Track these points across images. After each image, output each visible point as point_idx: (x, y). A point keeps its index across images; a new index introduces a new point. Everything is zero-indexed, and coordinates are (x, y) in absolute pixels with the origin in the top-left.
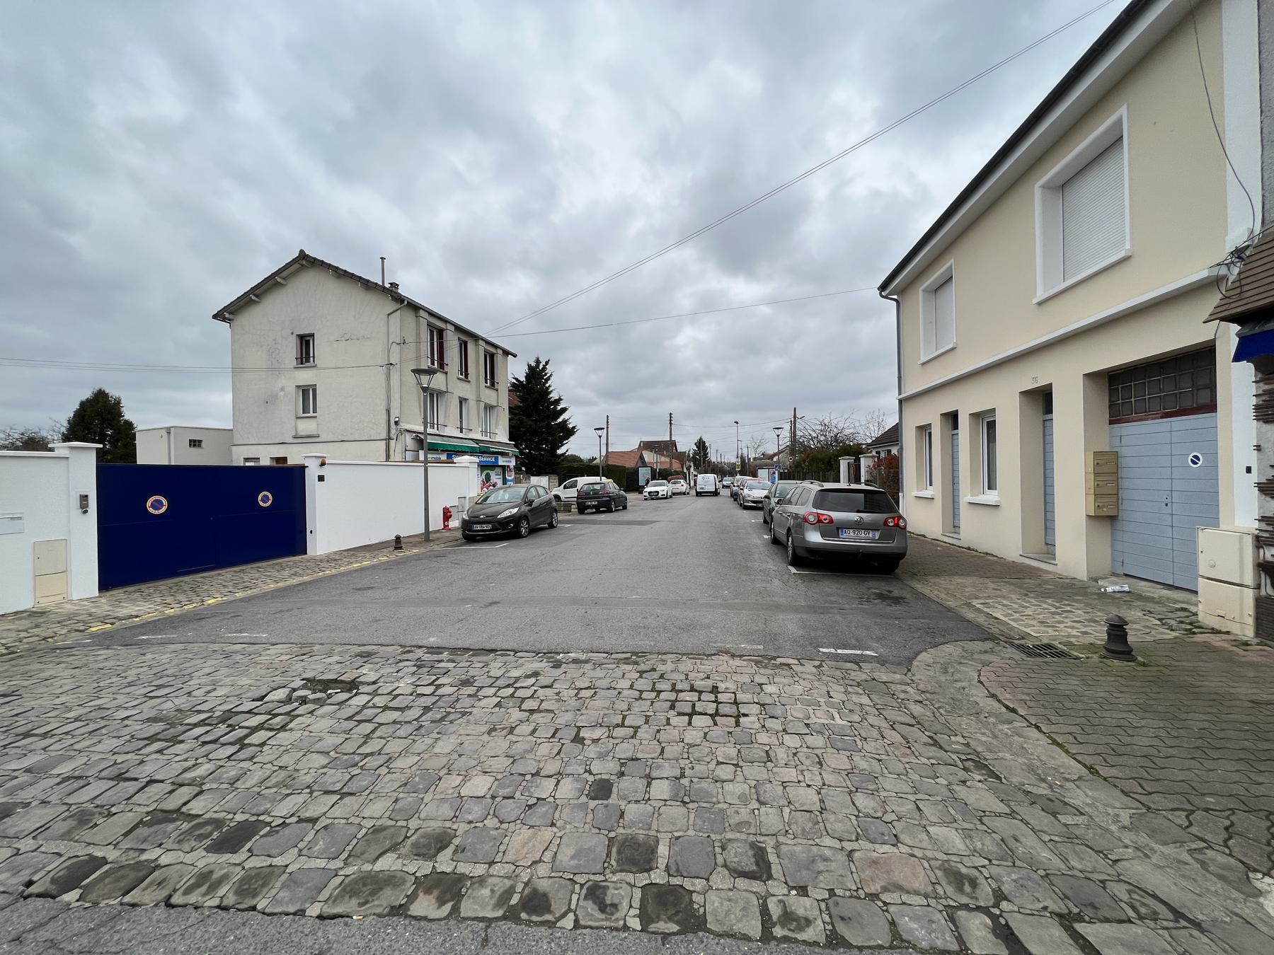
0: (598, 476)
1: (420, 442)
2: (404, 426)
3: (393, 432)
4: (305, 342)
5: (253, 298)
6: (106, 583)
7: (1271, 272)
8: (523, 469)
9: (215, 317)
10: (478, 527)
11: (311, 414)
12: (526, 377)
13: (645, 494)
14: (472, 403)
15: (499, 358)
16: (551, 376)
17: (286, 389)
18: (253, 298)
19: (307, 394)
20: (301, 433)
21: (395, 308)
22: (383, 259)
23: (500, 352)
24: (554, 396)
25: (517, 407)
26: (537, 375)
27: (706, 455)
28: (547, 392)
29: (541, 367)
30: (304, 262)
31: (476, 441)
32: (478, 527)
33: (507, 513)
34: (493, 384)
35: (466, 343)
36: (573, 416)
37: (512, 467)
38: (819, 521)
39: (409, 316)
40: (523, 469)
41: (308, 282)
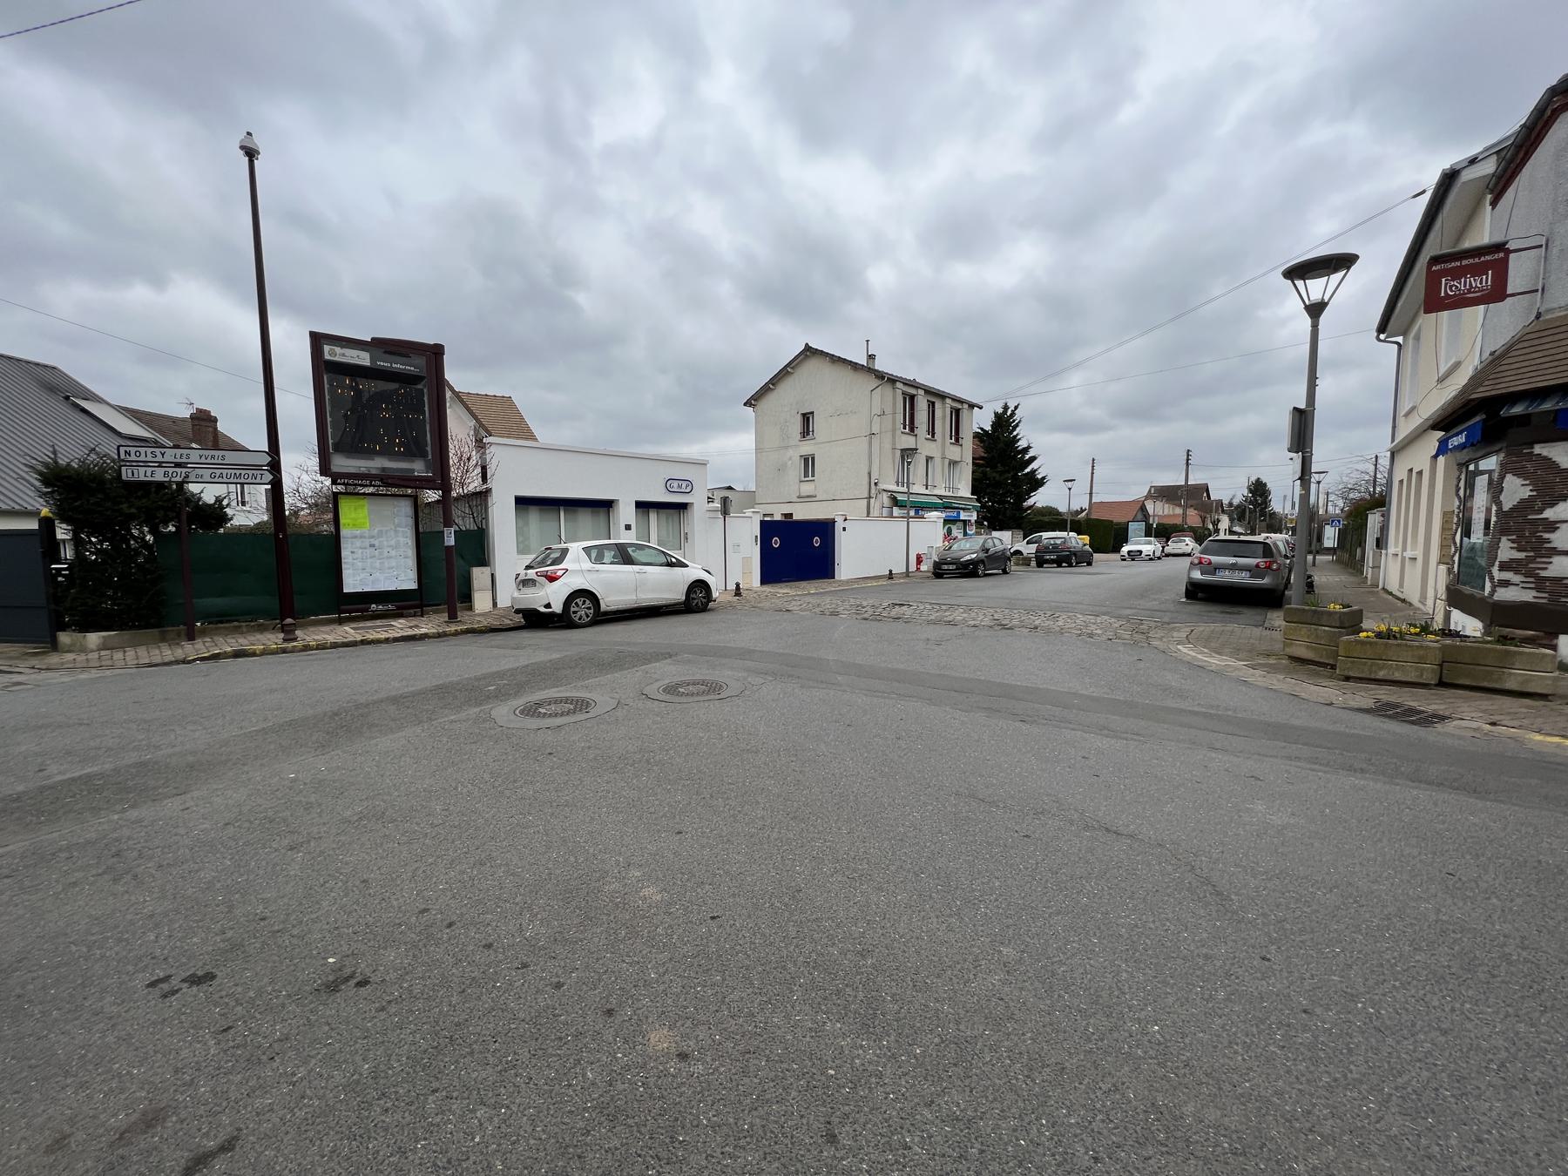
0: (1066, 531)
1: (895, 502)
2: (881, 486)
3: (873, 491)
4: (807, 418)
5: (771, 386)
6: (764, 581)
7: (1566, 374)
8: (986, 523)
9: (745, 404)
10: (946, 567)
11: (810, 478)
12: (992, 426)
13: (1122, 553)
14: (938, 461)
15: (964, 414)
16: (1019, 422)
17: (793, 458)
18: (771, 386)
19: (808, 462)
20: (802, 494)
21: (876, 385)
22: (868, 341)
23: (966, 406)
24: (1022, 444)
25: (982, 458)
26: (1004, 422)
27: (1266, 503)
28: (1015, 440)
29: (1009, 412)
30: (809, 352)
31: (940, 497)
32: (946, 567)
33: (968, 558)
34: (957, 440)
35: (933, 403)
36: (1041, 467)
37: (973, 521)
38: (1200, 563)
39: (888, 389)
40: (986, 523)
41: (813, 366)
